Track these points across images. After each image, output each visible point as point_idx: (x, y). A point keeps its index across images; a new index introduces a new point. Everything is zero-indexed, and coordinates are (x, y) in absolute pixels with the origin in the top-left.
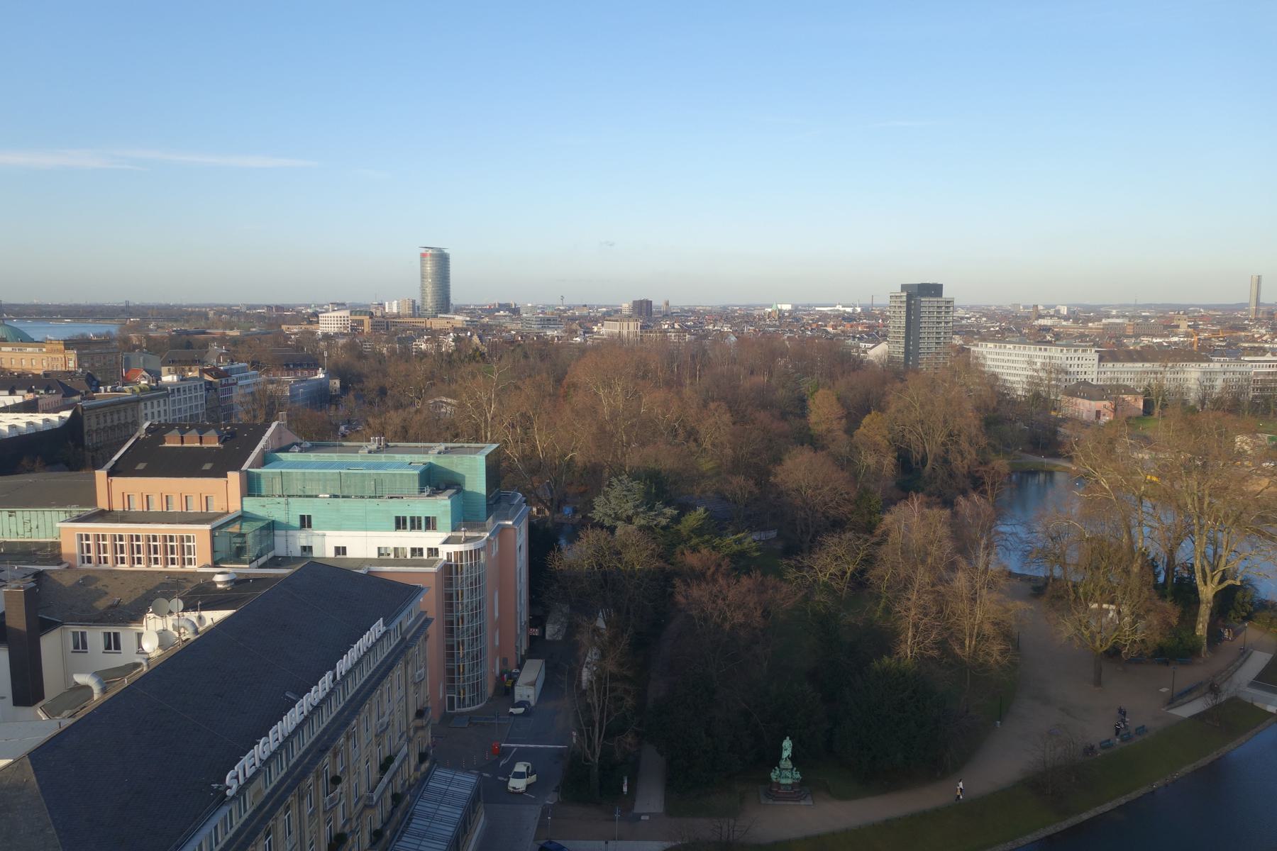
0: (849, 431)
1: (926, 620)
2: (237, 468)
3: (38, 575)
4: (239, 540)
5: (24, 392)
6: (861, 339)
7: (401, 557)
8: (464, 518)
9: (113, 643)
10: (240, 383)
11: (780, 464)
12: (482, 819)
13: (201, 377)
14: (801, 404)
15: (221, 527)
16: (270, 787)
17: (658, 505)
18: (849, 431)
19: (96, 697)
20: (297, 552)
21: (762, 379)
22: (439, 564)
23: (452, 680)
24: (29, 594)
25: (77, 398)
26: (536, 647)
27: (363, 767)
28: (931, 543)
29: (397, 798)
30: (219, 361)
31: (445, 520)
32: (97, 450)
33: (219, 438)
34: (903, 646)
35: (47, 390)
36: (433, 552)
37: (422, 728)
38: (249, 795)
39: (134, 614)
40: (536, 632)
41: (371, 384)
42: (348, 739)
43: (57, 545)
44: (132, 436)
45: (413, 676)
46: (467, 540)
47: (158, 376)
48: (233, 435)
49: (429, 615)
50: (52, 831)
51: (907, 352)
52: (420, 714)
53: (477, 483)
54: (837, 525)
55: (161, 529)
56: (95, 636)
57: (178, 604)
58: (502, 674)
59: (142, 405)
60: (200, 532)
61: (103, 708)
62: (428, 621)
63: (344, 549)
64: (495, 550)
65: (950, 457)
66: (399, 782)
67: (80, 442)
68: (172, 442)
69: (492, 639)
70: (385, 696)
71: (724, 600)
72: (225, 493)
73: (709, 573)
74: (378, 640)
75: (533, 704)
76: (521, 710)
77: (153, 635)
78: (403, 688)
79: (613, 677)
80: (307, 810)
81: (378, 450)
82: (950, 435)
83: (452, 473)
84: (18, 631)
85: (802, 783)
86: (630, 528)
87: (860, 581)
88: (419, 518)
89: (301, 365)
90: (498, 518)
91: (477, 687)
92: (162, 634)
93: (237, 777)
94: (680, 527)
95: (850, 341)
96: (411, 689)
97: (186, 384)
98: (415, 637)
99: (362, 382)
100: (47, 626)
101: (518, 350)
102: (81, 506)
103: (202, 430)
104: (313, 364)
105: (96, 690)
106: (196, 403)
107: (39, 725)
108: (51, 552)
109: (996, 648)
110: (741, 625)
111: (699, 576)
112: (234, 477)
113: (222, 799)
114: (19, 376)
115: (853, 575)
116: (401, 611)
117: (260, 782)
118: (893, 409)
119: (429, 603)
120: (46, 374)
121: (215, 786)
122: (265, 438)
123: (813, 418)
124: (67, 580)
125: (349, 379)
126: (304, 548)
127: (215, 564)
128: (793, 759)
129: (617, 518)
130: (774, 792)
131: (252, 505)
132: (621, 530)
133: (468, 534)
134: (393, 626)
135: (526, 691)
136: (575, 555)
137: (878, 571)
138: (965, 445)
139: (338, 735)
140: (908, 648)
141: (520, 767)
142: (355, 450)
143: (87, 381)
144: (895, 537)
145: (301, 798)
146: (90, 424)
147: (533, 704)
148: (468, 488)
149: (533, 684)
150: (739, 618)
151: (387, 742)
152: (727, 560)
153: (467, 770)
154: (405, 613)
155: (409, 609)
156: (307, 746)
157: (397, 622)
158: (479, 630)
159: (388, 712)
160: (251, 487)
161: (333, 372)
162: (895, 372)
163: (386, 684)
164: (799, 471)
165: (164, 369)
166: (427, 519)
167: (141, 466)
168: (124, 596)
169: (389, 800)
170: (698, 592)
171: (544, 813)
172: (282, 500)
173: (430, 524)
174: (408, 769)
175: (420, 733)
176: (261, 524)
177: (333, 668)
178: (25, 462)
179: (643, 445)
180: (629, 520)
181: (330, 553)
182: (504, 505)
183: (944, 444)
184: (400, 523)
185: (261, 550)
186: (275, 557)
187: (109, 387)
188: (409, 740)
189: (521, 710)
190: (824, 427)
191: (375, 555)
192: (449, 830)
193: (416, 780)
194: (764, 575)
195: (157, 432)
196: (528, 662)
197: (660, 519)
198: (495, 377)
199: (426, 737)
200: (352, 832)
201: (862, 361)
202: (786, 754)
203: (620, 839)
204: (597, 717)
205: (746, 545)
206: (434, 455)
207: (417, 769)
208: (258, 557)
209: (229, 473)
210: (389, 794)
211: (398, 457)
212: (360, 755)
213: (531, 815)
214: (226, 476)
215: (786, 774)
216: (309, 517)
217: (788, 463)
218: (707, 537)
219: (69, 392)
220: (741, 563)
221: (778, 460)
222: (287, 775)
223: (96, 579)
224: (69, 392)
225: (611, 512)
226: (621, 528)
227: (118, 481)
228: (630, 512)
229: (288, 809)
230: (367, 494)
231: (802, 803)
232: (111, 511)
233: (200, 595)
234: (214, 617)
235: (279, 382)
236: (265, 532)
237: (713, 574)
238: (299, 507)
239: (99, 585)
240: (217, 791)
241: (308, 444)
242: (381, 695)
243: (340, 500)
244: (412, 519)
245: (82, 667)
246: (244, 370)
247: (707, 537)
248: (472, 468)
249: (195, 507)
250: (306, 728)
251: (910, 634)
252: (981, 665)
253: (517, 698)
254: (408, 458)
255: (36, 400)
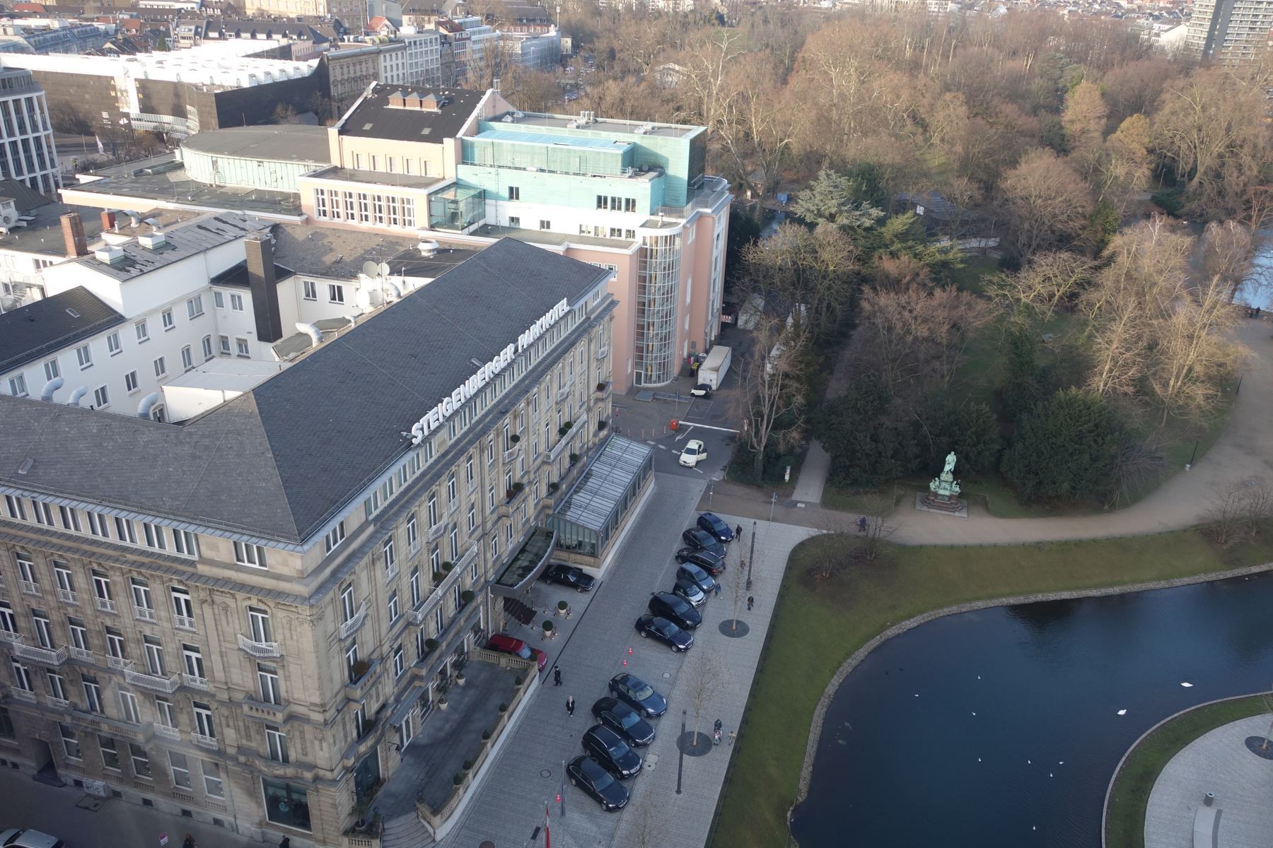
0: (1108, 131)
1: (1128, 355)
2: (452, 134)
3: (275, 228)
4: (453, 206)
5: (279, 37)
6: (1156, 18)
7: (601, 236)
8: (665, 203)
9: (337, 295)
10: (474, 38)
11: (1015, 168)
12: (652, 485)
13: (437, 30)
14: (1056, 100)
15: (436, 192)
16: (454, 439)
17: (865, 204)
18: (1108, 131)
19: (314, 344)
20: (505, 222)
21: (1024, 64)
22: (635, 247)
23: (641, 358)
24: (265, 245)
25: (326, 45)
26: (727, 334)
27: (543, 429)
28: (1160, 272)
29: (574, 458)
30: (454, 13)
31: (644, 205)
32: (342, 100)
33: (438, 103)
34: (1096, 379)
35: (299, 36)
36: (631, 233)
37: (602, 400)
38: (435, 442)
39: (350, 271)
40: (728, 319)
41: (601, 45)
42: (528, 404)
43: (297, 196)
44: (359, 96)
45: (596, 352)
46: (664, 225)
47: (397, 24)
48: (450, 100)
49: (615, 298)
50: (270, 455)
51: (1210, 39)
52: (601, 387)
53: (679, 167)
54: (1063, 241)
55: (385, 191)
56: (323, 287)
57: (385, 268)
58: (689, 357)
59: (382, 56)
60: (419, 198)
61: (315, 357)
62: (614, 303)
63: (548, 223)
64: (691, 238)
65: (1225, 171)
66: (578, 444)
67: (326, 92)
68: (395, 104)
69: (682, 323)
70: (567, 369)
71: (910, 312)
72: (437, 158)
73: (905, 281)
74: (561, 319)
75: (714, 388)
76: (702, 392)
77: (373, 291)
78: (585, 363)
79: (786, 375)
80: (487, 462)
81: (586, 126)
82: (1230, 146)
83: (655, 155)
84: (259, 278)
85: (961, 496)
86: (832, 226)
87: (1069, 304)
88: (620, 200)
89: (534, 20)
90: (698, 204)
91: (663, 366)
92: (372, 294)
93: (422, 429)
94: (883, 229)
95: (1142, 21)
96: (594, 365)
97: (423, 37)
98: (600, 317)
99: (592, 42)
100: (283, 274)
101: (759, 13)
102: (316, 161)
103: (423, 93)
104: (546, 21)
105: (315, 338)
106: (430, 58)
107: (268, 362)
108: (290, 203)
109: (1199, 393)
110: (924, 339)
111: (894, 284)
112: (449, 143)
113: (409, 446)
114: (275, 20)
115: (1061, 298)
116: (586, 292)
117: (444, 434)
118: (1167, 109)
119: (620, 284)
120: (299, 19)
121: (404, 434)
122: (479, 106)
123: (1068, 116)
124: (300, 234)
125: (581, 37)
126: (512, 219)
127: (432, 227)
128: (956, 473)
129: (820, 215)
130: (931, 500)
131: (466, 173)
132: (820, 227)
133: (666, 219)
134: (576, 307)
135: (709, 375)
136: (777, 245)
137: (1093, 296)
138: (1246, 159)
139: (518, 400)
140: (1100, 383)
141: (693, 444)
142: (564, 124)
143: (335, 27)
144: (1124, 260)
145: (482, 451)
146: (335, 74)
147: (714, 388)
148: (671, 171)
149: (717, 370)
150: (923, 332)
151: (567, 410)
152: (926, 270)
153: (644, 442)
154: (591, 294)
155: (595, 290)
156: (489, 407)
157: (582, 302)
158: (669, 314)
159: (568, 384)
160: (465, 155)
161: (566, 30)
162: (1184, 64)
163: (569, 358)
164: (1037, 178)
165: (405, 19)
166: (628, 201)
167: (368, 127)
168: (344, 251)
169: (567, 460)
170: (886, 300)
171: (709, 487)
172: (493, 170)
173: (631, 205)
174: (587, 433)
175: (600, 404)
176: (473, 192)
177: (515, 341)
178: (279, 109)
179: (865, 134)
180: (832, 218)
181: (536, 227)
182: (706, 191)
183: (1220, 156)
184: (601, 202)
185: (474, 217)
186: (486, 225)
187: (352, 37)
188: (589, 410)
189: (702, 392)
190: (1078, 126)
191: (577, 232)
192: (618, 492)
193: (594, 444)
194: (960, 290)
195: (383, 92)
196: (716, 348)
197: (864, 219)
198: (724, 46)
199: (607, 409)
200: (530, 483)
201: (1151, 46)
202: (947, 468)
203: (774, 520)
204: (766, 411)
205: (951, 256)
206: (639, 135)
207: (595, 435)
208: (470, 224)
209: (445, 140)
210: (567, 454)
211: (604, 134)
212: (540, 420)
213: (697, 487)
214: (442, 142)
215: (944, 485)
216: (517, 189)
217: (1023, 168)
218: (910, 243)
219: (319, 39)
220: (942, 273)
221: (1013, 163)
222: (470, 430)
223: (324, 236)
224: (319, 39)
225: (812, 208)
226: (823, 226)
227: (347, 139)
228: (833, 210)
229: (470, 458)
230: (571, 171)
231: (957, 514)
232: (342, 168)
233: (406, 263)
234: (417, 283)
235: (511, 38)
236: (476, 200)
237: (908, 284)
238: (509, 179)
239: (326, 241)
240: (405, 438)
241: (521, 114)
242: (563, 368)
243: (546, 174)
244: (613, 200)
245: (308, 311)
246: (477, 24)
247: (910, 243)
248: (675, 151)
249: (415, 171)
250: (488, 391)
251: (1107, 368)
252: (1180, 407)
253: (700, 381)
254: (613, 136)
255: (289, 46)
